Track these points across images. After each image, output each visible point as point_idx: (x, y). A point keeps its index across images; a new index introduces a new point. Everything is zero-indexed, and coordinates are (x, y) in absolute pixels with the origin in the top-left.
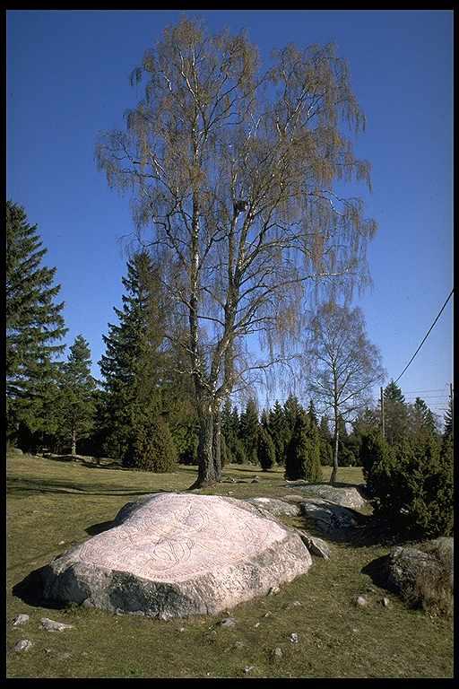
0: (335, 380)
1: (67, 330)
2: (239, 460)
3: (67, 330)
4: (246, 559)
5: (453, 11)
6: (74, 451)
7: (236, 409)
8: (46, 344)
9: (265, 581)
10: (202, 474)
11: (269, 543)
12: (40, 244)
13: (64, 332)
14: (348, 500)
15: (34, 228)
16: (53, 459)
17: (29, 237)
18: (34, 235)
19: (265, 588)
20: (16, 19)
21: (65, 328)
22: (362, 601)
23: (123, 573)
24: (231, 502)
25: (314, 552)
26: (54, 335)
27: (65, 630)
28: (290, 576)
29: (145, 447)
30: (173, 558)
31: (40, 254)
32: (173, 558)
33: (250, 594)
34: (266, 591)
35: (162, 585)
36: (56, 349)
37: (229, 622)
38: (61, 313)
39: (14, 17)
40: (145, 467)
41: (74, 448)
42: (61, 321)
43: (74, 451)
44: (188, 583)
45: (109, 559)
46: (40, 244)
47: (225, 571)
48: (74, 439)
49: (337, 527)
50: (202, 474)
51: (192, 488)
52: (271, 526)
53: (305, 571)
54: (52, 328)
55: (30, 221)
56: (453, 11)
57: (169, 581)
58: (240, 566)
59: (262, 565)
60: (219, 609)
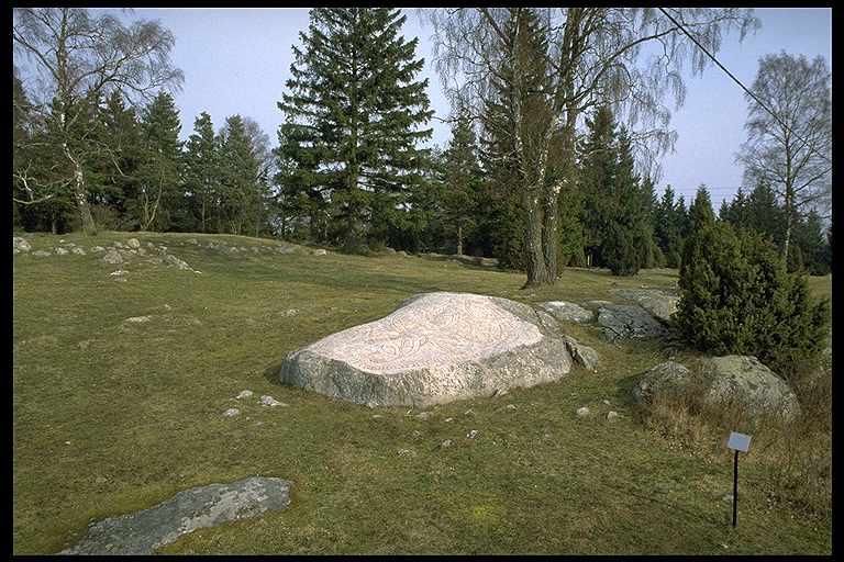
0: (789, 161)
1: (433, 112)
3: (433, 112)
4: (477, 360)
6: (460, 251)
7: (682, 200)
8: (411, 128)
9: (489, 383)
10: (531, 277)
11: (512, 346)
13: (429, 115)
16: (434, 259)
19: (489, 390)
21: (429, 110)
23: (340, 362)
25: (576, 360)
26: (419, 117)
28: (529, 381)
33: (470, 394)
34: (491, 392)
35: (370, 376)
36: (421, 134)
38: (426, 90)
41: (460, 247)
42: (426, 102)
43: (460, 251)
44: (397, 376)
47: (445, 368)
48: (460, 235)
50: (531, 277)
58: (464, 366)
60: (426, 403)
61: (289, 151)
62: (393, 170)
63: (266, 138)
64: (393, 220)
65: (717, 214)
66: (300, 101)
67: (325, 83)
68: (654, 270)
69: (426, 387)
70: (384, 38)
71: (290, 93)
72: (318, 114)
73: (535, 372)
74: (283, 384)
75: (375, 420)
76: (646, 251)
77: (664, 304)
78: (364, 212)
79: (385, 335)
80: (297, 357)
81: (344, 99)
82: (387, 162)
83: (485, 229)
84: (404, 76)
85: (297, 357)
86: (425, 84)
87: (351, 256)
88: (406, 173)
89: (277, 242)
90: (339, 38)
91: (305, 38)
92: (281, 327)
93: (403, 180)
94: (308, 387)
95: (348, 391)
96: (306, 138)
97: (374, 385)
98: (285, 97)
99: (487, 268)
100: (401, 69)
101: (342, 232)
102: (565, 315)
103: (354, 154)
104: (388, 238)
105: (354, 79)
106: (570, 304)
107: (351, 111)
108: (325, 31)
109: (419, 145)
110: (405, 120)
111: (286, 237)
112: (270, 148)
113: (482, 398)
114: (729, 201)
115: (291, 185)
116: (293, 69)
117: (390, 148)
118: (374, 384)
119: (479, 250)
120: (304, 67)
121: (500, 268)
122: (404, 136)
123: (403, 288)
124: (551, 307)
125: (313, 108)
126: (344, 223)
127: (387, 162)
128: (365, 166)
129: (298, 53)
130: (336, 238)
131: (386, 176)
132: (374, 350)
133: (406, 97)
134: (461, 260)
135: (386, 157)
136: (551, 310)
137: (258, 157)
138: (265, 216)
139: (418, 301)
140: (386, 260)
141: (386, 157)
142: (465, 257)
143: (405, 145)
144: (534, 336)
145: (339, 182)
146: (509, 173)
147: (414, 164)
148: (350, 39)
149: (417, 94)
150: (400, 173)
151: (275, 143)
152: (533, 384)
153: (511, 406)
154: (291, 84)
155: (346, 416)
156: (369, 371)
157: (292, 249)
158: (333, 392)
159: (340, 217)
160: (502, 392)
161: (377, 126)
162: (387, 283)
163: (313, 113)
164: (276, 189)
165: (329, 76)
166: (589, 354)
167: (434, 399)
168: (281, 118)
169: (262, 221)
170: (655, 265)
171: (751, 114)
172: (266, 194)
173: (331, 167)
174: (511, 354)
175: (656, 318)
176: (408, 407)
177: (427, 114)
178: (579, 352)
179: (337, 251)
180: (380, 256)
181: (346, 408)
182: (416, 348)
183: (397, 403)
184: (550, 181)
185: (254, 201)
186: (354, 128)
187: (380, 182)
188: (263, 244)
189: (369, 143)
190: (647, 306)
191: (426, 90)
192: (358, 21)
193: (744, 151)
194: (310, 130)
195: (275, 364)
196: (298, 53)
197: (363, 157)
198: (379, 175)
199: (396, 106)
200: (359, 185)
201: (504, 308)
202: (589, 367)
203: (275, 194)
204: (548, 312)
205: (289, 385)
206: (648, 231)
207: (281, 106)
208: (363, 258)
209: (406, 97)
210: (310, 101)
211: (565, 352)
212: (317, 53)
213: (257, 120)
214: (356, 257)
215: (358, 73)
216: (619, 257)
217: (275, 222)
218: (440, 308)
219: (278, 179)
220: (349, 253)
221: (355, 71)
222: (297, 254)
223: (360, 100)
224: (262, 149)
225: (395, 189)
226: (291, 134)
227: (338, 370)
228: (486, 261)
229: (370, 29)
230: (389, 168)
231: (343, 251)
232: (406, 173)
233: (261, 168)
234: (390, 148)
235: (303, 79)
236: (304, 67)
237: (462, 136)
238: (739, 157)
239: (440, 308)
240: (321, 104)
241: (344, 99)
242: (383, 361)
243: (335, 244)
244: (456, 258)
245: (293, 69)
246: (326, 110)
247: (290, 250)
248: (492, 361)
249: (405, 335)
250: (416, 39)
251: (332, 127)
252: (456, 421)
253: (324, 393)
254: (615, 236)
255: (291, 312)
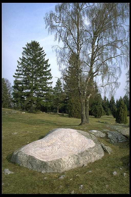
1: (52, 77)
2: (108, 114)
3: (52, 77)
4: (77, 154)
5: (2, 3)
6: (58, 112)
7: (108, 99)
9: (82, 162)
11: (87, 148)
12: (44, 53)
13: (51, 78)
14: (126, 132)
15: (42, 48)
17: (41, 51)
18: (42, 50)
19: (81, 165)
20: (5, 5)
21: (52, 76)
22: (115, 173)
23: (32, 156)
24: (79, 132)
25: (105, 151)
26: (49, 79)
27: (10, 174)
28: (93, 160)
29: (75, 111)
30: (51, 152)
31: (44, 56)
32: (51, 152)
33: (75, 166)
35: (43, 162)
37: (62, 177)
38: (50, 72)
39: (5, 5)
40: (75, 117)
41: (58, 111)
44: (51, 162)
45: (30, 151)
46: (44, 53)
47: (67, 158)
48: (58, 108)
49: (118, 142)
51: (79, 125)
52: (91, 142)
53: (100, 158)
54: (48, 77)
55: (41, 46)
56: (2, 3)
57: (45, 161)
58: (73, 156)
59: (82, 156)
60: (62, 171)
61: (16, 87)
62: (42, 92)
63: (10, 84)
64: (42, 104)
65: (116, 102)
66: (19, 74)
67: (25, 70)
68: (104, 116)
69: (62, 165)
70: (41, 59)
71: (17, 73)
72: (23, 78)
73: (95, 156)
74: (13, 162)
75: (45, 180)
76: (102, 112)
77: (124, 130)
78: (35, 102)
79: (46, 145)
80: (17, 154)
81: (30, 74)
82: (41, 90)
83: (65, 106)
84: (45, 68)
85: (17, 154)
86: (50, 70)
87: (31, 114)
88: (45, 92)
89: (12, 110)
90: (29, 59)
91: (21, 59)
92: (12, 139)
93: (45, 94)
94: (21, 165)
95: (35, 167)
96: (20, 84)
97: (44, 165)
98: (16, 74)
99: (65, 116)
100: (44, 66)
101: (29, 107)
102: (98, 135)
103: (32, 88)
104: (40, 109)
105: (33, 69)
106: (98, 131)
107: (32, 77)
108: (26, 57)
109: (49, 86)
110: (46, 79)
111: (15, 108)
112: (11, 86)
113: (80, 168)
114: (118, 99)
115: (16, 95)
116: (18, 66)
117: (41, 86)
118: (44, 165)
119: (63, 112)
120: (20, 66)
121: (69, 117)
122: (45, 83)
123: (46, 124)
124: (93, 132)
125: (22, 76)
126: (30, 105)
127: (41, 90)
128: (35, 91)
129: (19, 62)
130: (27, 108)
131: (40, 93)
132: (43, 151)
133: (45, 73)
134: (58, 114)
135: (41, 89)
136: (93, 133)
137: (8, 88)
138: (10, 102)
139: (55, 132)
140: (40, 115)
141: (41, 89)
142: (59, 113)
143: (45, 86)
144: (91, 144)
145: (28, 95)
146: (70, 93)
147: (47, 90)
148: (32, 59)
149: (48, 73)
150: (44, 93)
151: (13, 84)
152: (94, 161)
153: (90, 171)
154: (17, 70)
155: (34, 177)
156: (42, 160)
157: (16, 111)
158: (30, 167)
159: (29, 103)
160: (86, 165)
161: (38, 81)
162: (42, 122)
163: (22, 78)
164: (12, 96)
165: (26, 68)
166: (108, 149)
167: (64, 169)
168: (14, 79)
169: (9, 104)
170: (104, 115)
171: (127, 79)
172: (10, 97)
173: (27, 91)
174: (87, 151)
175: (123, 135)
176: (56, 173)
177: (51, 78)
178: (106, 149)
179: (28, 112)
180: (38, 114)
181: (34, 174)
182: (57, 150)
183: (52, 171)
184: (88, 95)
185: (7, 99)
186: (32, 81)
187: (39, 95)
188: (8, 110)
189: (36, 85)
190: (119, 131)
191: (50, 72)
192: (34, 55)
193: (126, 88)
194: (21, 82)
195: (10, 154)
196: (19, 62)
197: (34, 88)
198: (38, 93)
199: (43, 76)
200: (34, 95)
201: (81, 134)
202: (110, 153)
203: (12, 97)
204: (93, 134)
205: (15, 163)
206: (101, 106)
207: (14, 76)
208: (34, 114)
209: (45, 73)
210: (22, 74)
211: (102, 149)
212: (23, 62)
213: (8, 79)
214: (33, 114)
215: (34, 67)
216: (97, 113)
217: (12, 104)
218: (62, 134)
219: (13, 93)
220: (31, 113)
221: (33, 67)
222: (17, 113)
223: (34, 74)
224: (9, 86)
225: (42, 96)
226: (17, 83)
227: (31, 159)
228: (65, 114)
229: (37, 57)
230: (41, 91)
231: (29, 112)
232: (45, 92)
233: (9, 91)
234: (41, 86)
235: (20, 69)
236: (20, 66)
237: (59, 83)
238: (125, 89)
239: (62, 134)
240: (24, 75)
241: (30, 74)
242: (46, 155)
243: (27, 110)
244: (57, 114)
245: (18, 66)
246: (26, 77)
247: (16, 112)
248: (81, 154)
249: (53, 145)
250: (48, 59)
251: (27, 81)
252: (74, 180)
253: (26, 167)
254: (95, 108)
255: (15, 133)
